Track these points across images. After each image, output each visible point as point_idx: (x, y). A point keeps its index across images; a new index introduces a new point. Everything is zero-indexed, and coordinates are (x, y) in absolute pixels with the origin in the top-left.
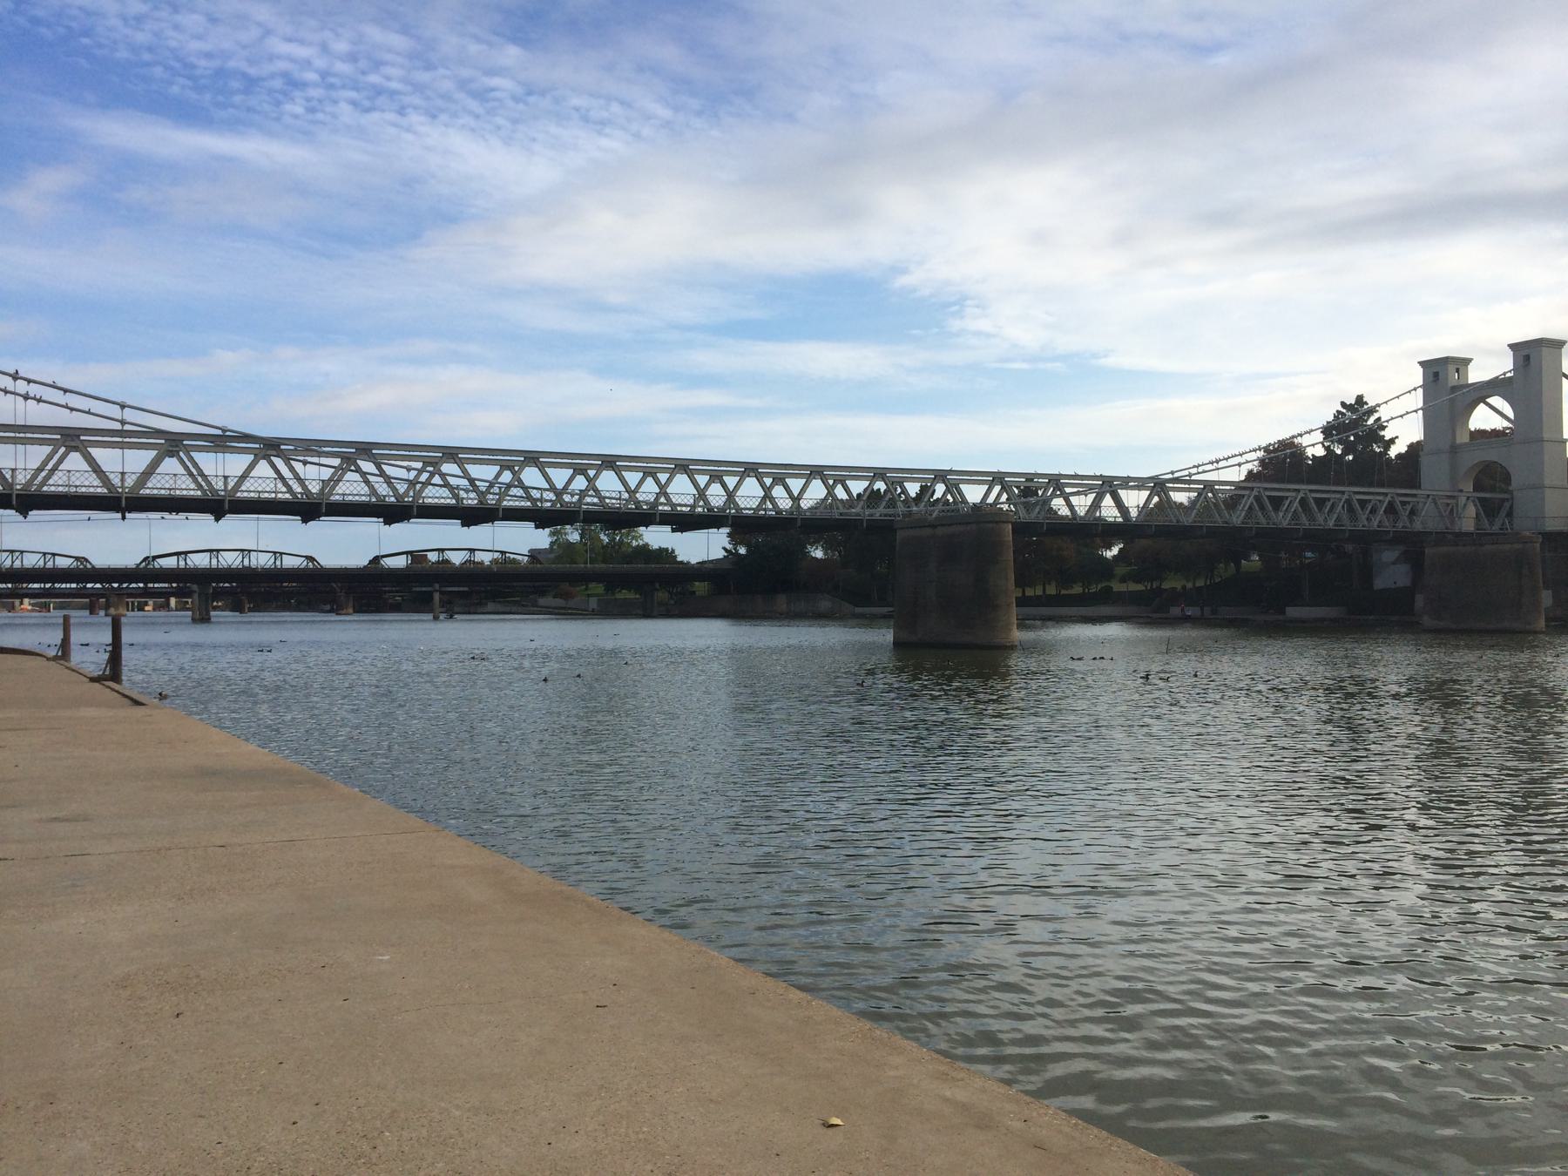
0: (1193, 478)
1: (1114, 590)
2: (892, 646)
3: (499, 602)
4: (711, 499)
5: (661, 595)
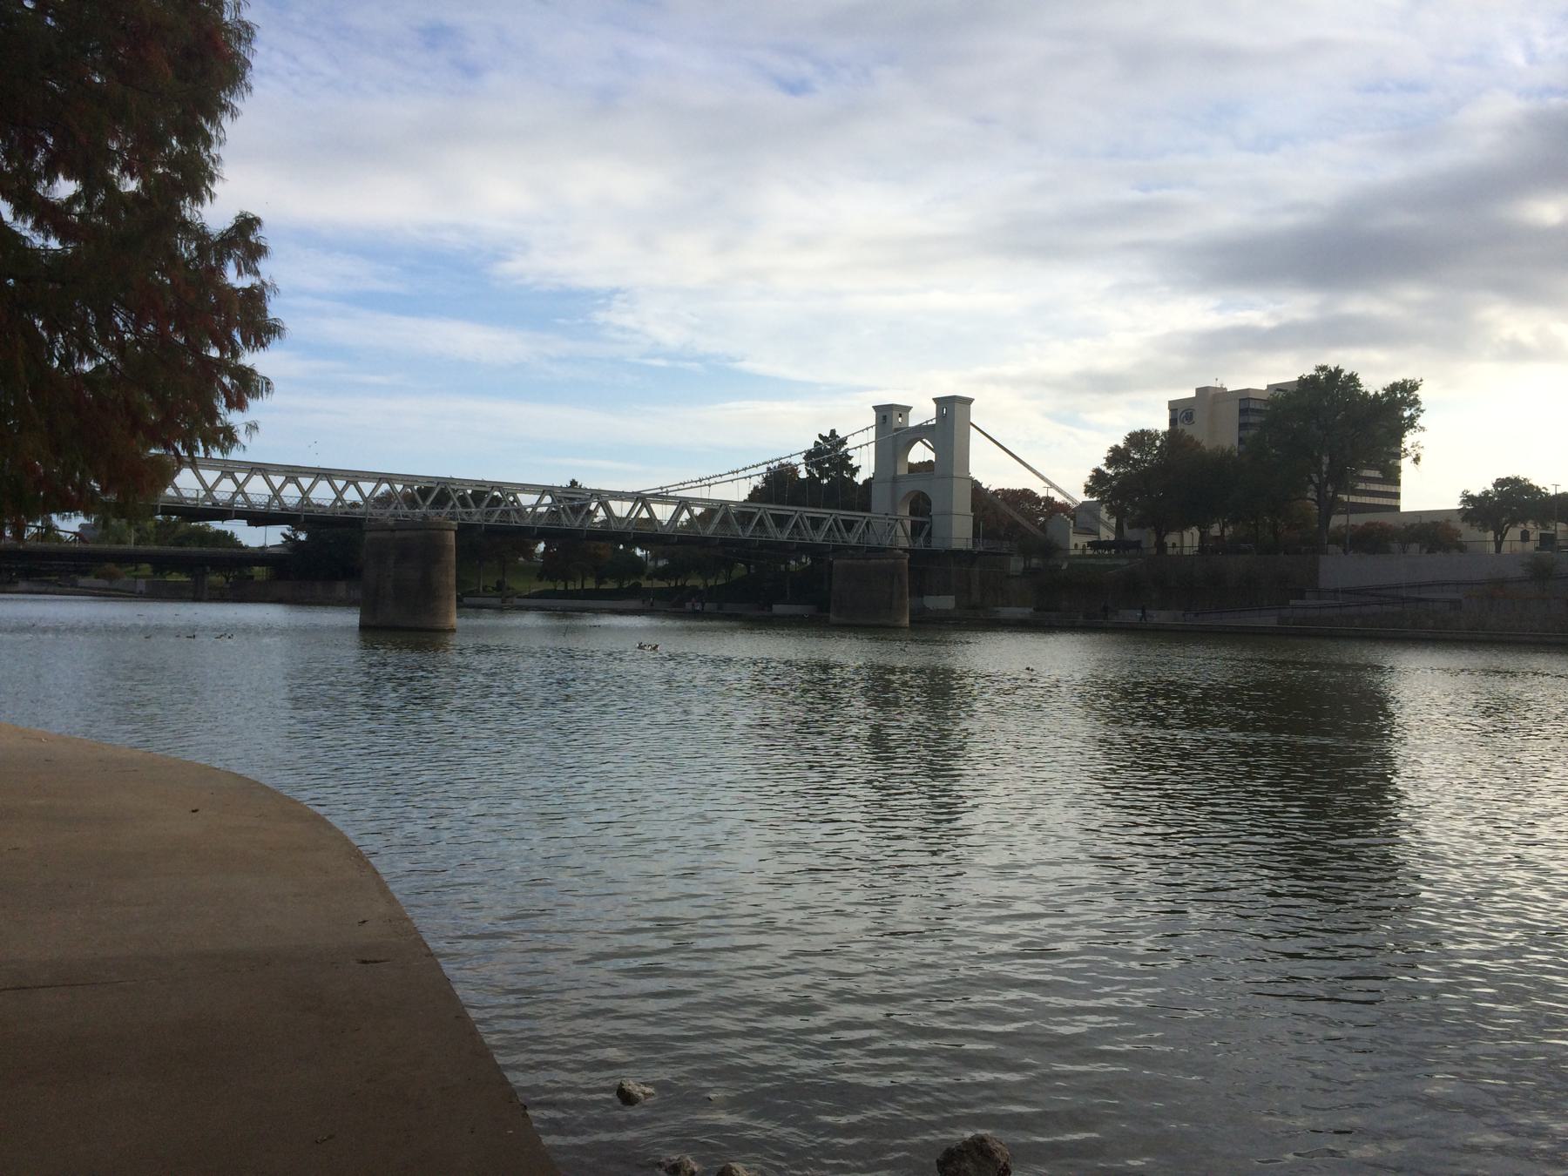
0: (670, 494)
1: (643, 586)
2: (358, 629)
3: (33, 581)
4: (285, 499)
5: (216, 579)
